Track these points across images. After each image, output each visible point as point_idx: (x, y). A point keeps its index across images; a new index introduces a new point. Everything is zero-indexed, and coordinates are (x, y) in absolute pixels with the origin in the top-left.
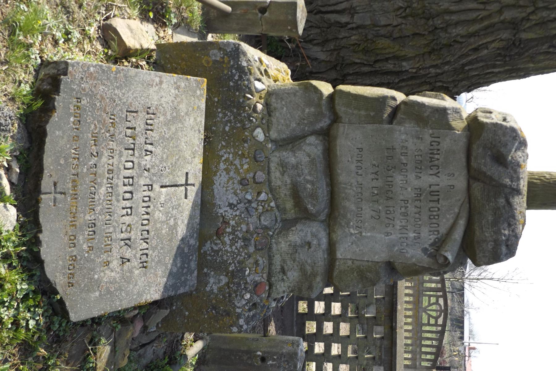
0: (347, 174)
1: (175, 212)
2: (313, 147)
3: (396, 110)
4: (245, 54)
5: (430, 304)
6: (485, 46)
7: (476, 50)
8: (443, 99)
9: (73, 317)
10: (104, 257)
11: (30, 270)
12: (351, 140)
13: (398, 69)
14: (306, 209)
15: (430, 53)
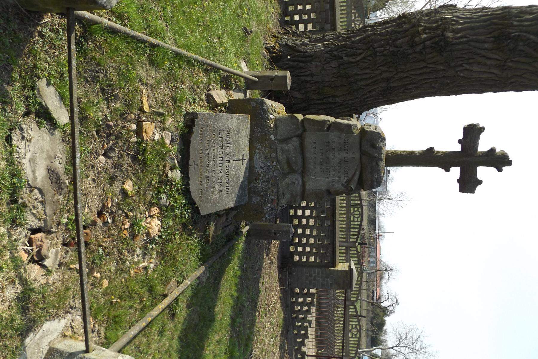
0: (310, 154)
1: (239, 171)
2: (295, 142)
3: (330, 126)
4: (265, 103)
5: (354, 211)
6: (374, 90)
7: (370, 92)
8: (351, 120)
9: (202, 213)
10: (212, 190)
11: (186, 195)
12: (311, 139)
13: (334, 101)
14: (293, 168)
15: (349, 94)
